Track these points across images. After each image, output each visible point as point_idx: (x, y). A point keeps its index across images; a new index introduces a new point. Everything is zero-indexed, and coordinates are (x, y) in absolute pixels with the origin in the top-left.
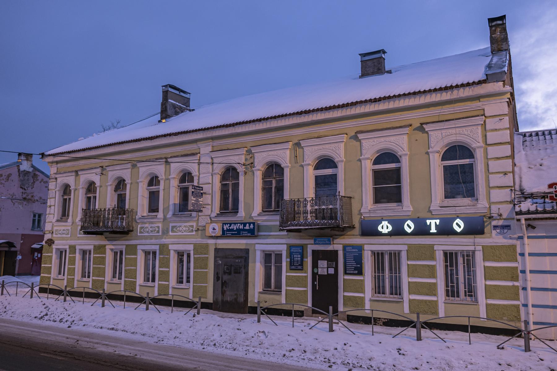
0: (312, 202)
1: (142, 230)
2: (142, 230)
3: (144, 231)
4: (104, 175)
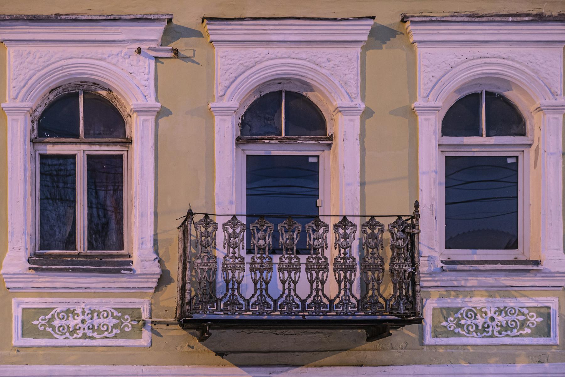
0: (231, 231)
1: (451, 323)
2: (451, 323)
3: (459, 325)
4: (185, 58)
